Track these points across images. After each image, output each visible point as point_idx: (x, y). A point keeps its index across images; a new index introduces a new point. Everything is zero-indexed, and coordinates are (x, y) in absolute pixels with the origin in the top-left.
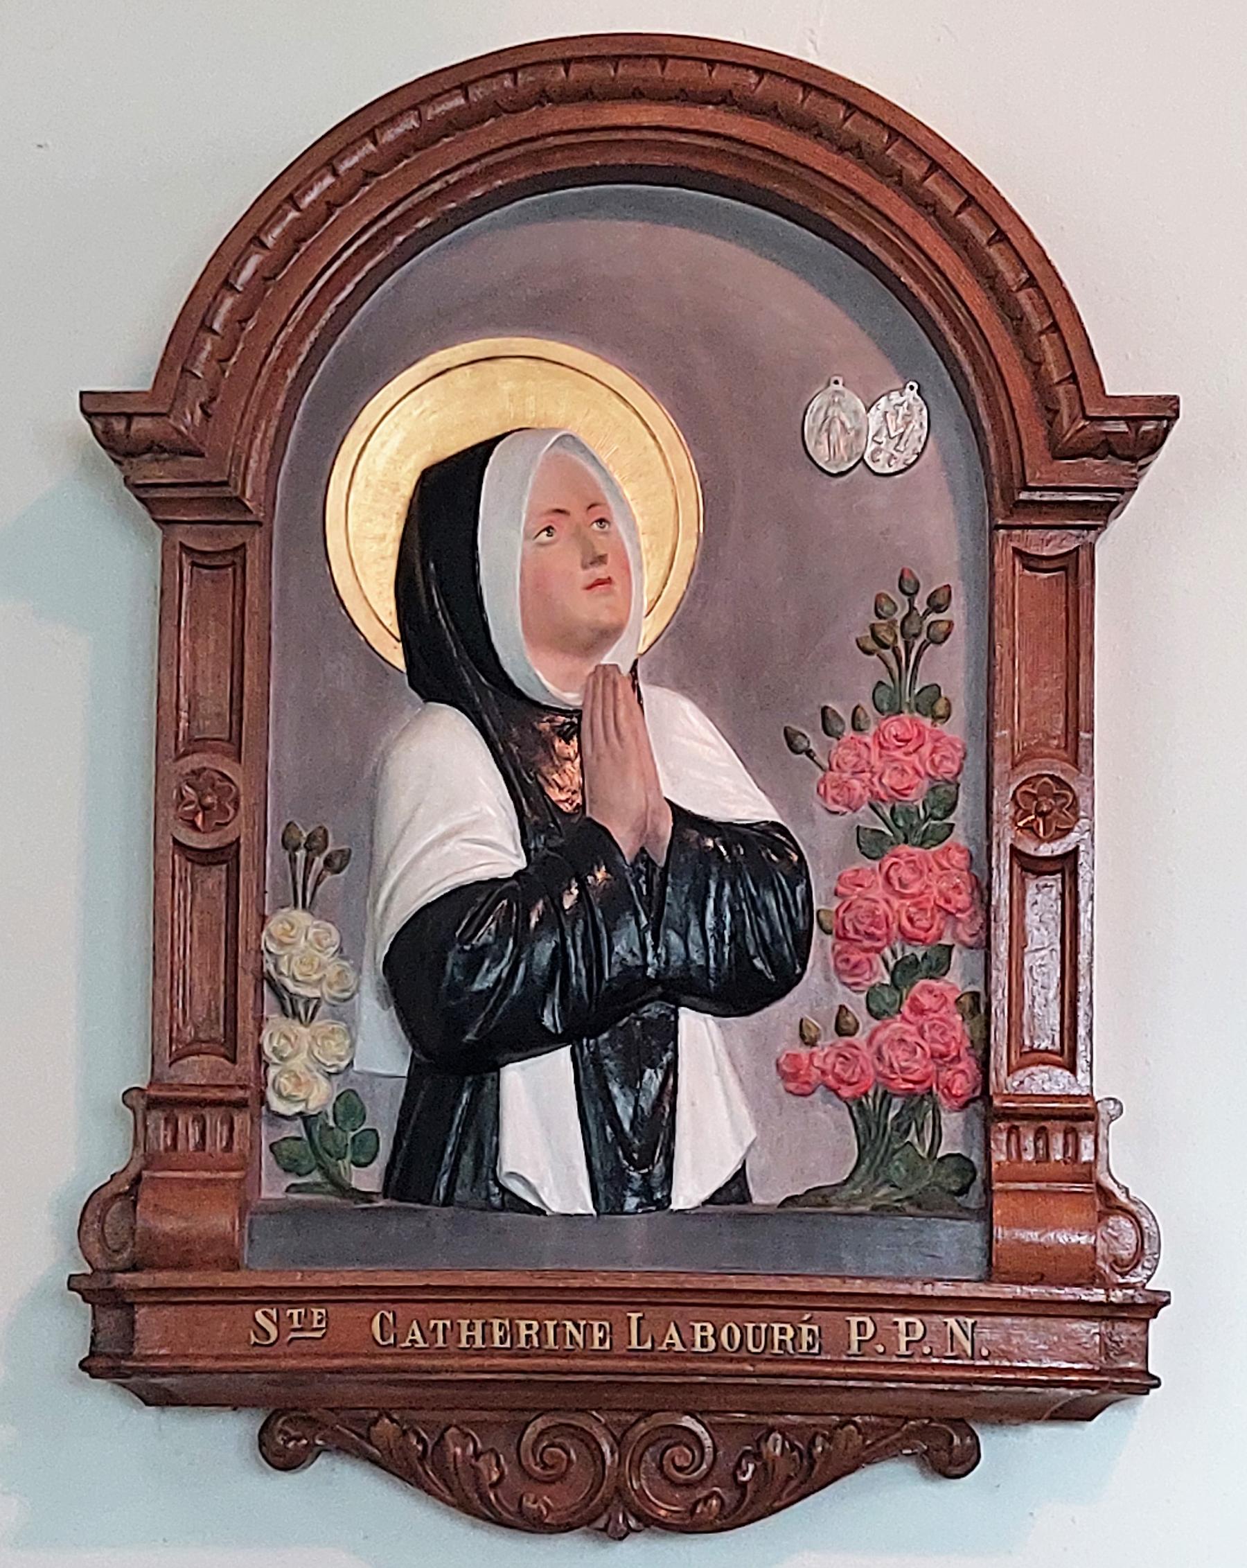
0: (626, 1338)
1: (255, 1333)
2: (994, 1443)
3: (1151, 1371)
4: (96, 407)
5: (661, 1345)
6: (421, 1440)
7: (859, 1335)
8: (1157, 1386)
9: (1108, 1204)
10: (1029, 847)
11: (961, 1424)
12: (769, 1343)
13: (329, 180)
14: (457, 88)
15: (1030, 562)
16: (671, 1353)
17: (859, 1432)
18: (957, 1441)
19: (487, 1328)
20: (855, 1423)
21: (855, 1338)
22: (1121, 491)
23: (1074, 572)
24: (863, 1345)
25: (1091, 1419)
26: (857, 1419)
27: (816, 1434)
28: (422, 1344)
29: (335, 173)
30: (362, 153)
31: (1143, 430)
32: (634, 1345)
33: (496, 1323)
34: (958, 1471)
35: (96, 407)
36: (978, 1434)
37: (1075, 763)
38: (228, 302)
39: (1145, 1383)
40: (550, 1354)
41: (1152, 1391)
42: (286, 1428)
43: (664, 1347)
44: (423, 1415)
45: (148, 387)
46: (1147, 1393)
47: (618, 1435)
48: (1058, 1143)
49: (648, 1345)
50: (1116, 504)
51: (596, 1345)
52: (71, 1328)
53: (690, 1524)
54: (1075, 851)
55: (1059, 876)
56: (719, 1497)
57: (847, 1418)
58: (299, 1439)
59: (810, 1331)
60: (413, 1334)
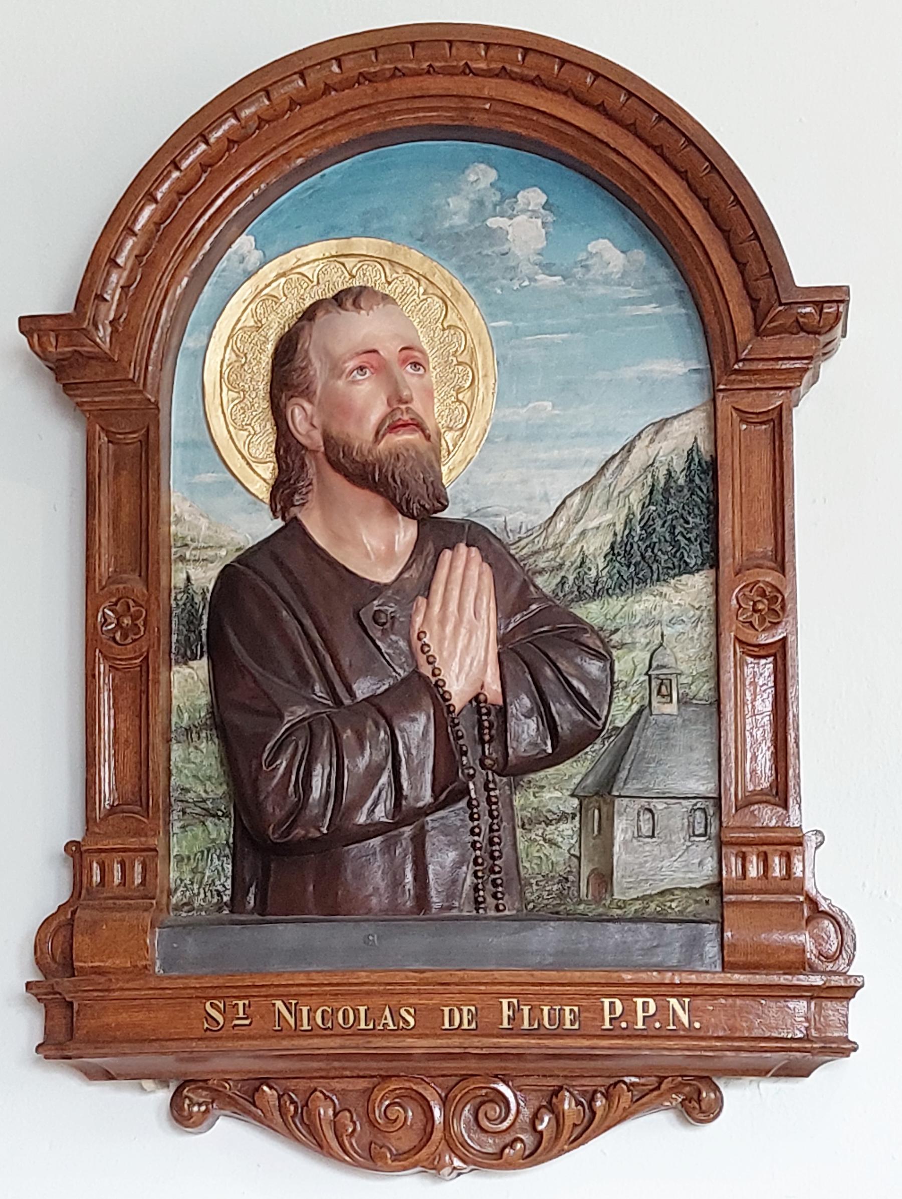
0: (440, 1020)
1: (207, 1020)
2: (736, 1095)
3: (851, 1038)
4: (30, 325)
5: (379, 1025)
6: (293, 1102)
7: (644, 1012)
8: (855, 1050)
9: (816, 910)
10: (749, 635)
11: (707, 1079)
12: (561, 1022)
13: (203, 147)
14: (295, 73)
15: (744, 416)
16: (386, 1032)
17: (629, 1090)
18: (704, 1095)
19: (562, 1012)
20: (625, 1083)
21: (640, 1014)
22: (810, 358)
23: (778, 427)
24: (646, 1019)
25: (807, 1076)
26: (627, 1079)
27: (595, 1092)
28: (392, 1027)
29: (207, 142)
30: (225, 127)
31: (824, 313)
32: (447, 1026)
33: (567, 1009)
34: (701, 1117)
35: (30, 325)
36: (722, 1089)
37: (784, 573)
38: (130, 242)
39: (843, 1048)
40: (529, 1034)
41: (853, 1054)
42: (190, 1095)
43: (381, 1027)
44: (337, 1085)
45: (69, 308)
46: (848, 1056)
47: (443, 1095)
48: (777, 862)
49: (371, 1026)
50: (806, 370)
51: (568, 1026)
52: (26, 1024)
53: (497, 1161)
54: (784, 639)
55: (771, 659)
56: (522, 1141)
57: (617, 1079)
58: (200, 1105)
59: (469, 1010)
60: (386, 1019)
